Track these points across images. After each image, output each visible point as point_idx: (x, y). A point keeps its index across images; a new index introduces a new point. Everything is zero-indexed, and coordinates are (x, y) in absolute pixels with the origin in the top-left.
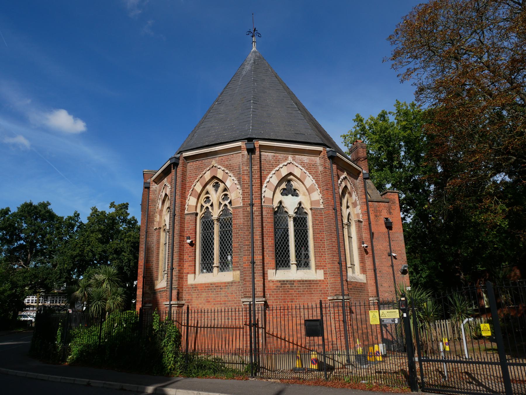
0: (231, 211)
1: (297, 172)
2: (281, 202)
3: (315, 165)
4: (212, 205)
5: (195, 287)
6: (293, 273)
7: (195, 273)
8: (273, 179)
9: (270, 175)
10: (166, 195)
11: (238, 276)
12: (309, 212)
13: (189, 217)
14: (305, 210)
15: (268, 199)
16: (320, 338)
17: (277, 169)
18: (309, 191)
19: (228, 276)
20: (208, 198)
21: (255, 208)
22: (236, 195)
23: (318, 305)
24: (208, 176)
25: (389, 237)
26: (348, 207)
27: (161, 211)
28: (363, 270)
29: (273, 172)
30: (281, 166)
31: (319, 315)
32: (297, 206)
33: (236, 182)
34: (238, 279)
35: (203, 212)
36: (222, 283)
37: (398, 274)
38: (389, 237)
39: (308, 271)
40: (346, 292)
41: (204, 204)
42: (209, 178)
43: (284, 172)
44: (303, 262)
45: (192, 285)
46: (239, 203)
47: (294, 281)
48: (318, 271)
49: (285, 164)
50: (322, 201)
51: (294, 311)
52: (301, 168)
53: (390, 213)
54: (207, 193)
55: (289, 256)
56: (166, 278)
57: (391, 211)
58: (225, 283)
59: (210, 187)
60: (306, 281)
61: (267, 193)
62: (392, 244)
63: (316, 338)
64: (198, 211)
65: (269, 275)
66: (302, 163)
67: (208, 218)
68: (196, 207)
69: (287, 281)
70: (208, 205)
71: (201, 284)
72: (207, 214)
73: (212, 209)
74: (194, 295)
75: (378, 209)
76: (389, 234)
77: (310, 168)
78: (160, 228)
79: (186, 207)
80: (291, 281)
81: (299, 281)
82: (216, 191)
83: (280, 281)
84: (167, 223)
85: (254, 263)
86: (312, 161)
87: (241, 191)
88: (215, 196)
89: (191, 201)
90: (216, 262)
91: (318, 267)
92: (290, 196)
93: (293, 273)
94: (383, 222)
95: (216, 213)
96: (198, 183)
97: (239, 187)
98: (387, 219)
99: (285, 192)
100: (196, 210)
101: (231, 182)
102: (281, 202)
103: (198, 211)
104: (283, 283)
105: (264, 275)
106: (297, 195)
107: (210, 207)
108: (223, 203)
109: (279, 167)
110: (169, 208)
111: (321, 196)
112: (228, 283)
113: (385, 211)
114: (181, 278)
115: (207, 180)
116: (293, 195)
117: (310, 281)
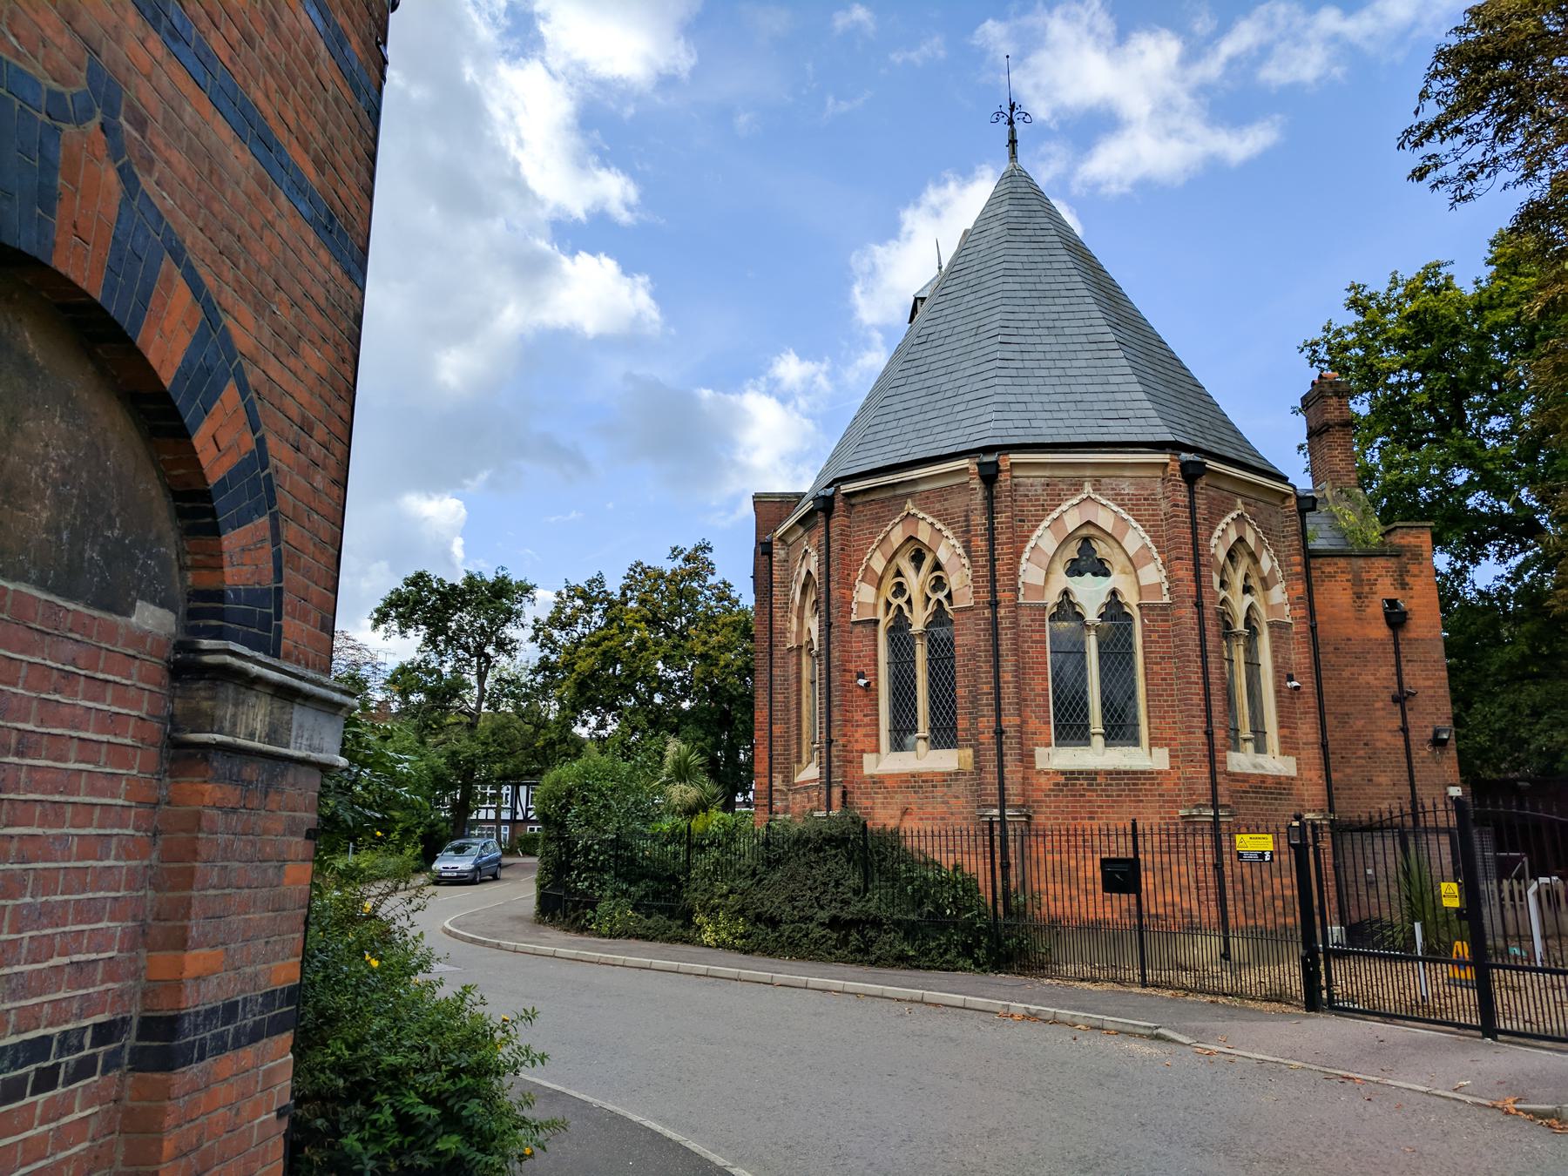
0: (951, 615)
1: (1105, 520)
2: (1066, 592)
3: (1150, 499)
4: (909, 602)
5: (878, 781)
6: (1097, 756)
7: (877, 750)
8: (1044, 539)
9: (1038, 532)
10: (809, 572)
11: (970, 760)
12: (1136, 613)
13: (858, 629)
14: (1127, 609)
15: (1035, 587)
16: (1133, 896)
17: (1055, 515)
18: (1134, 564)
19: (948, 760)
20: (900, 585)
21: (1002, 612)
22: (959, 579)
23: (1129, 828)
24: (897, 536)
25: (1397, 652)
26: (1247, 589)
27: (802, 608)
28: (1288, 746)
29: (1046, 523)
30: (1064, 507)
31: (1130, 849)
32: (1104, 599)
33: (960, 551)
34: (969, 767)
35: (891, 615)
36: (935, 774)
37: (1423, 752)
38: (1397, 652)
39: (1132, 749)
40: (1223, 800)
41: (892, 600)
42: (901, 541)
43: (1072, 521)
44: (1119, 729)
45: (872, 777)
46: (965, 598)
47: (1096, 773)
48: (1154, 750)
49: (1075, 501)
50: (1166, 586)
51: (1096, 839)
52: (1116, 508)
53: (1404, 586)
54: (899, 573)
55: (1086, 716)
56: (816, 760)
57: (1407, 579)
58: (943, 774)
59: (905, 564)
60: (1126, 772)
61: (1030, 573)
62: (1406, 669)
63: (1124, 896)
64: (880, 615)
65: (1037, 758)
66: (1118, 498)
67: (902, 629)
68: (875, 606)
69: (1081, 773)
70: (901, 601)
71: (892, 776)
72: (899, 627)
73: (911, 611)
74: (879, 799)
75: (1365, 576)
76: (1396, 644)
77: (1134, 505)
78: (800, 648)
79: (854, 606)
80: (1089, 773)
81: (1109, 773)
82: (918, 569)
83: (1063, 773)
84: (815, 636)
85: (1002, 732)
86: (1143, 488)
87: (970, 572)
88: (915, 582)
89: (865, 593)
90: (923, 727)
91: (1154, 742)
92: (1089, 575)
93: (1097, 756)
94: (1380, 612)
95: (918, 620)
96: (878, 554)
97: (966, 561)
98: (1392, 603)
99: (1075, 569)
100: (875, 612)
101: (948, 550)
102: (1066, 592)
103: (880, 615)
104: (1071, 775)
105: (1027, 758)
106: (1107, 574)
107: (905, 607)
108: (934, 597)
109: (1059, 510)
110: (816, 602)
111: (1164, 573)
112: (950, 774)
113: (1388, 581)
114: (852, 760)
115: (896, 546)
116: (1095, 574)
117: (1135, 772)
